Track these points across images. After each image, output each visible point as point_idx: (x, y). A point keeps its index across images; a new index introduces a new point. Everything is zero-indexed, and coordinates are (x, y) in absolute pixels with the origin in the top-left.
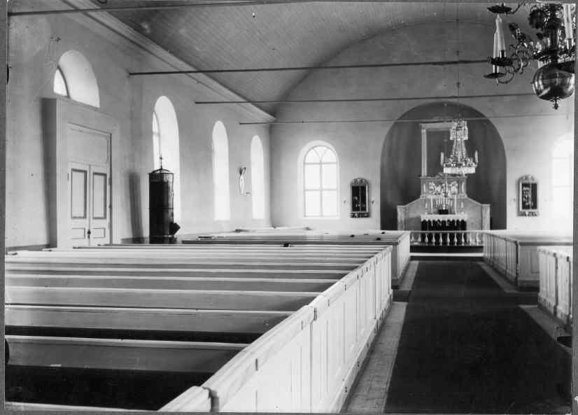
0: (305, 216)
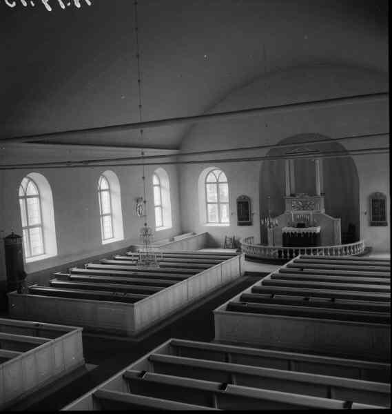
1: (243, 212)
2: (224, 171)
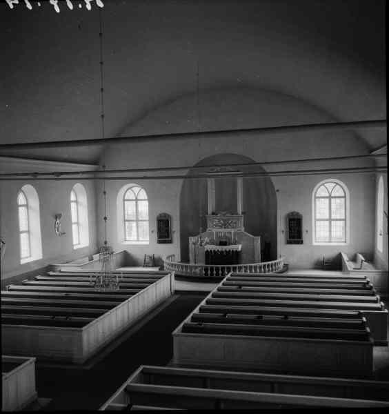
1: (163, 230)
2: (143, 187)
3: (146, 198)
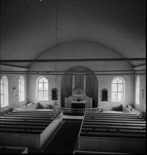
0: (38, 98)
1: (54, 95)
3: (48, 82)
